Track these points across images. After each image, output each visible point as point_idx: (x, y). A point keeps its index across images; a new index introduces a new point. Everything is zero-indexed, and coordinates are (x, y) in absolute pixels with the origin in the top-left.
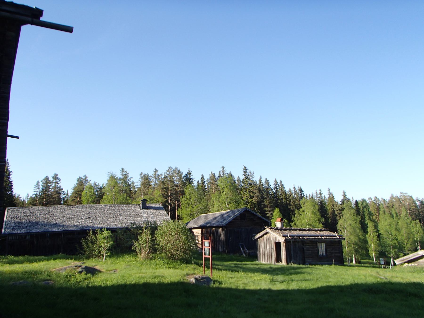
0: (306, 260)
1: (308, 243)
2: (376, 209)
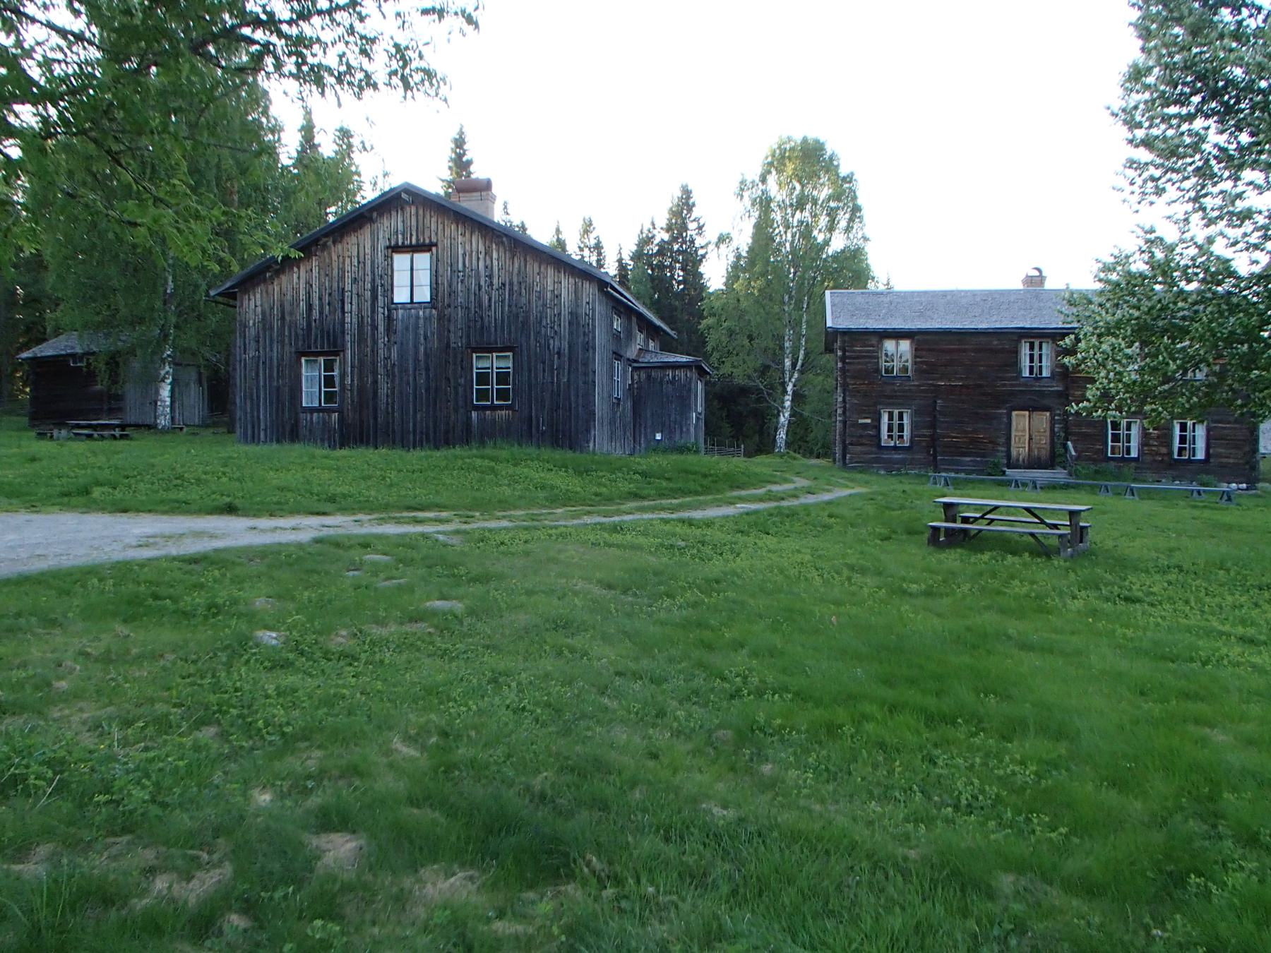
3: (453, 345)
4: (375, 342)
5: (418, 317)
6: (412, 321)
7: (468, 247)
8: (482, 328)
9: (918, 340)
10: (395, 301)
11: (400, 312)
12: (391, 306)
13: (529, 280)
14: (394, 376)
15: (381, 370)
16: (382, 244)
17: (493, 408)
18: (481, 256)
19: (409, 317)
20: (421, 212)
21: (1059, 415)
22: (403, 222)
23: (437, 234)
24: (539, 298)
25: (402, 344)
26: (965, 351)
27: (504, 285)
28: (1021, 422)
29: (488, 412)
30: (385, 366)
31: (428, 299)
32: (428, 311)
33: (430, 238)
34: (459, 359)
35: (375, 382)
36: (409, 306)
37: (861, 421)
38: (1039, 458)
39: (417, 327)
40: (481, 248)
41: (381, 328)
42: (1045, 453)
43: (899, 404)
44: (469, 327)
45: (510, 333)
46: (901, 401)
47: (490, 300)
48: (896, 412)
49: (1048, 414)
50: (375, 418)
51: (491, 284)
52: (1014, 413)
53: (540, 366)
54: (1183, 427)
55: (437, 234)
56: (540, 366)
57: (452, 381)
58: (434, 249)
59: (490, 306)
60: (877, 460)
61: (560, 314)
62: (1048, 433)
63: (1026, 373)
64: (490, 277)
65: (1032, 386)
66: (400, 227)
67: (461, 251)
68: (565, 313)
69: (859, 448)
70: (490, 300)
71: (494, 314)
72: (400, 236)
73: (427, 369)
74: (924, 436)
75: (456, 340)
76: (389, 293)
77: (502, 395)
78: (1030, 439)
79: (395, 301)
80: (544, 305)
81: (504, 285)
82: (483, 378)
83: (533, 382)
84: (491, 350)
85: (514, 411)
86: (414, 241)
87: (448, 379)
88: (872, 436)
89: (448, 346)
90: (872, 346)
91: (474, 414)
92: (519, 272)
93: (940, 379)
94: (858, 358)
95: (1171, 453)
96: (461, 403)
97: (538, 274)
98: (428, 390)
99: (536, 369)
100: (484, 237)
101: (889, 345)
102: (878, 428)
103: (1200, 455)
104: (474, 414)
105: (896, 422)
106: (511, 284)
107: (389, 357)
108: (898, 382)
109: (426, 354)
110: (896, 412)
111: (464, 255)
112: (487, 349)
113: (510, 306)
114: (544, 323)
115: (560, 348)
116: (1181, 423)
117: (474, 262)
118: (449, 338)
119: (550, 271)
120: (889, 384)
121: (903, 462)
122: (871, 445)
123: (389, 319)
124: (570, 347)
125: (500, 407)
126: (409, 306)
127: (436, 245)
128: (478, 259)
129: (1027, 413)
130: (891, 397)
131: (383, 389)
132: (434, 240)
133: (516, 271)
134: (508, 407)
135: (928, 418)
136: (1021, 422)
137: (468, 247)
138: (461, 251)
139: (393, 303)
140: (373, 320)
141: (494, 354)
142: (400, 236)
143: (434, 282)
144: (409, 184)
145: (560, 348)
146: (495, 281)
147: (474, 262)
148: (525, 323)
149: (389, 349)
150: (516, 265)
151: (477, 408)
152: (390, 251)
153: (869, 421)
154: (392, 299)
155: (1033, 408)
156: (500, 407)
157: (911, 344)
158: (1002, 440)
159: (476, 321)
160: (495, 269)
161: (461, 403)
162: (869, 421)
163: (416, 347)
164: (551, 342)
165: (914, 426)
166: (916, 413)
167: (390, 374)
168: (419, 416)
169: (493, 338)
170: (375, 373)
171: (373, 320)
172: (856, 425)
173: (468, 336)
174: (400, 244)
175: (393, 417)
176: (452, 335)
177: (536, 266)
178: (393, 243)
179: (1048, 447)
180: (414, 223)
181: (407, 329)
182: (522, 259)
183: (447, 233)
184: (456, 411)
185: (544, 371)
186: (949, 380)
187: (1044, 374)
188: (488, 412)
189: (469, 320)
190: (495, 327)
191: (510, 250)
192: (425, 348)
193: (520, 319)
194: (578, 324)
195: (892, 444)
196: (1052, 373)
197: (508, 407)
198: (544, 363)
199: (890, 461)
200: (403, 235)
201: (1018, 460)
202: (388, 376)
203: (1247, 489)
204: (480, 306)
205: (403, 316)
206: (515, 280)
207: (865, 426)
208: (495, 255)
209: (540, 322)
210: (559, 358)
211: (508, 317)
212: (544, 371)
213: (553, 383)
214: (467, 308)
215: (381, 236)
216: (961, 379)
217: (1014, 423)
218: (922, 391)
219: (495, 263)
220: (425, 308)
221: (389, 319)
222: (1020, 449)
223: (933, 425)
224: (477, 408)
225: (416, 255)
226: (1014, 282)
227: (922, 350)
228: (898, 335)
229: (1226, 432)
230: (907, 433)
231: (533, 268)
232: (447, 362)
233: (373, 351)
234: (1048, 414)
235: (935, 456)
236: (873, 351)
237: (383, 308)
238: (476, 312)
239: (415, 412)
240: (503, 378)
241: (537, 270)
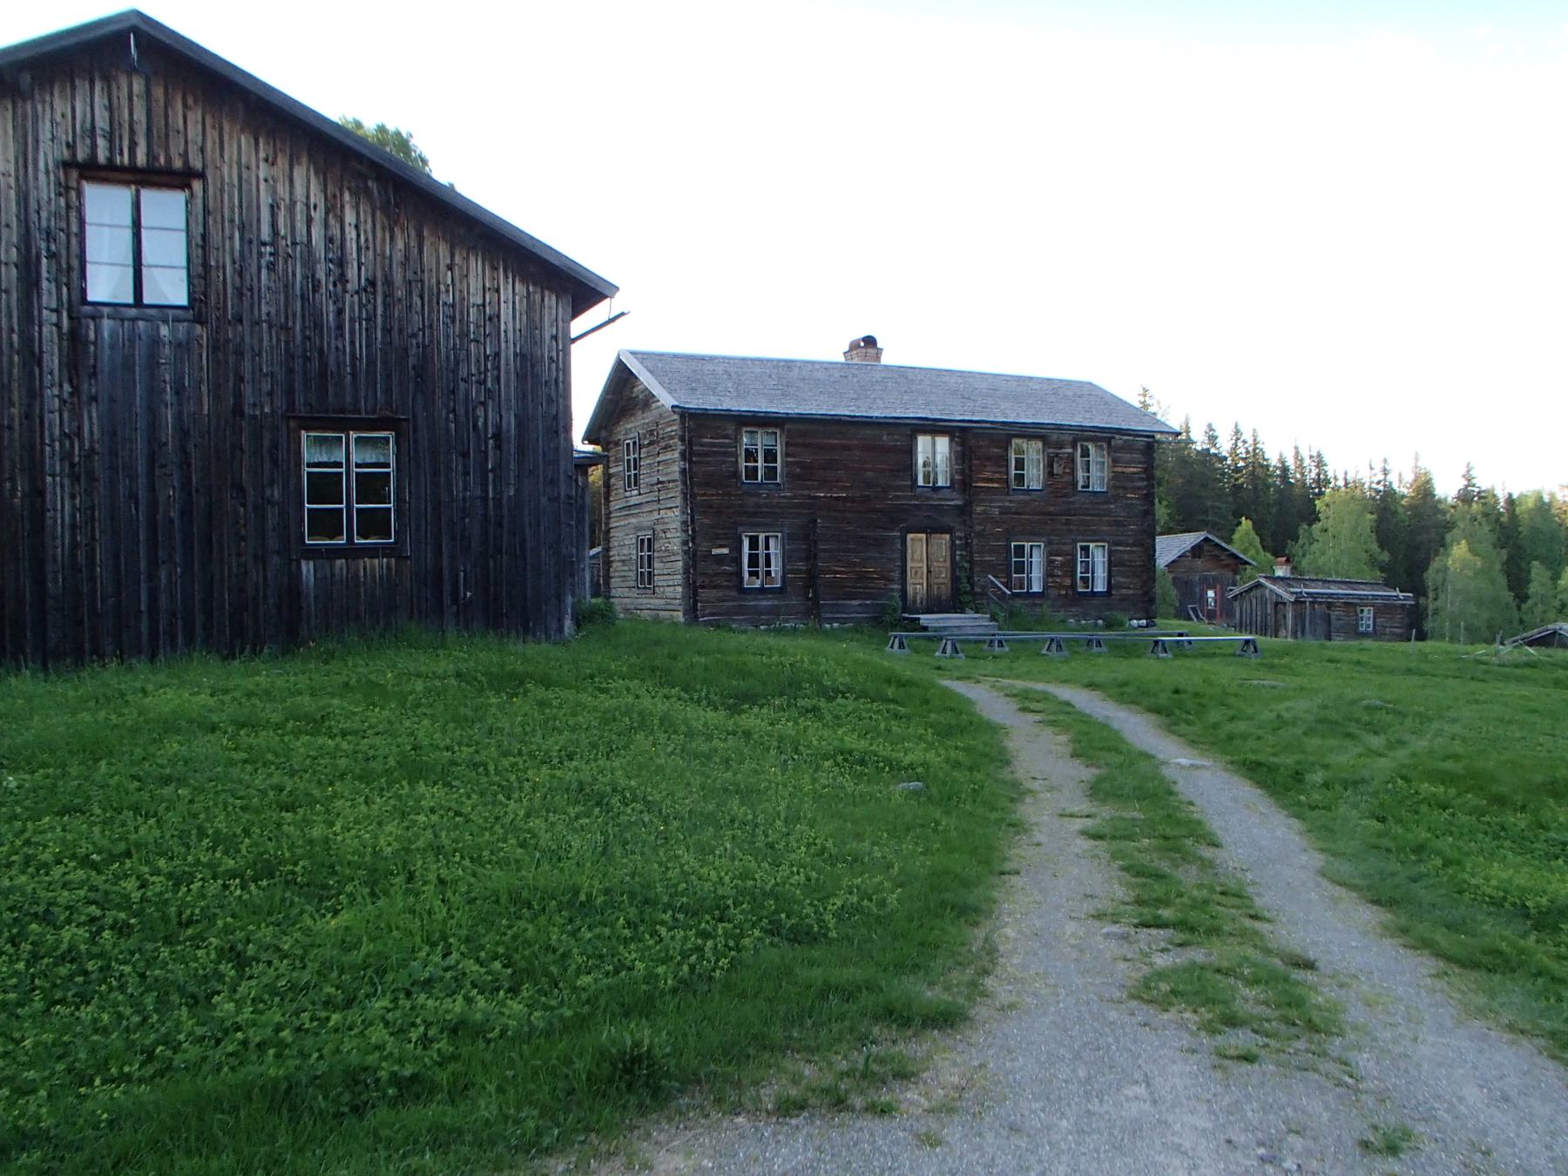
3: (248, 410)
4: (34, 394)
5: (156, 341)
6: (140, 351)
7: (282, 190)
8: (323, 374)
9: (789, 430)
10: (90, 298)
11: (107, 324)
12: (78, 306)
13: (430, 279)
14: (92, 478)
15: (53, 463)
16: (49, 154)
17: (351, 552)
18: (318, 216)
19: (133, 337)
20: (158, 92)
21: (960, 539)
22: (110, 108)
23: (202, 150)
24: (453, 320)
25: (112, 400)
26: (847, 448)
27: (372, 283)
28: (917, 544)
29: (340, 563)
30: (67, 456)
31: (183, 300)
32: (182, 328)
33: (185, 155)
34: (266, 443)
35: (38, 492)
36: (133, 312)
37: (715, 551)
38: (939, 598)
39: (153, 363)
40: (316, 197)
41: (52, 360)
42: (946, 591)
43: (766, 525)
44: (291, 371)
45: (388, 391)
46: (768, 520)
47: (340, 312)
48: (762, 536)
49: (948, 536)
50: (39, 580)
51: (342, 279)
52: (910, 536)
53: (456, 462)
54: (754, 543)
55: (202, 150)
56: (456, 462)
57: (251, 491)
58: (197, 185)
59: (340, 327)
60: (741, 610)
61: (497, 355)
62: (948, 564)
63: (921, 482)
64: (341, 263)
65: (928, 499)
66: (102, 122)
67: (265, 200)
68: (508, 352)
69: (714, 593)
70: (340, 312)
71: (355, 342)
72: (101, 143)
73: (185, 464)
74: (800, 571)
75: (259, 400)
76: (75, 275)
77: (373, 523)
78: (929, 572)
79: (90, 298)
80: (464, 335)
81: (372, 283)
82: (326, 486)
83: (444, 498)
84: (345, 425)
85: (400, 558)
86: (141, 159)
87: (240, 490)
88: (730, 574)
89: (238, 410)
90: (726, 437)
91: (307, 568)
92: (407, 258)
93: (819, 489)
94: (707, 454)
95: (1073, 586)
96: (272, 542)
97: (450, 268)
98: (186, 512)
99: (449, 469)
100: (323, 173)
101: (923, 442)
102: (738, 561)
103: (1100, 587)
104: (307, 568)
105: (761, 551)
106: (388, 282)
107: (79, 434)
108: (764, 493)
109: (183, 433)
110: (762, 536)
111: (274, 208)
112: (335, 421)
113: (387, 331)
114: (463, 372)
115: (499, 427)
116: (750, 537)
117: (301, 226)
118: (238, 395)
119: (476, 266)
120: (752, 495)
121: (774, 612)
122: (728, 587)
123: (75, 340)
124: (519, 424)
125: (372, 552)
126: (133, 312)
127: (202, 176)
128: (309, 221)
129: (924, 536)
130: (755, 514)
131: (61, 504)
132: (197, 164)
133: (398, 256)
134: (387, 551)
135: (804, 547)
136: (917, 544)
137: (282, 190)
138: (265, 200)
139: (84, 301)
140: (27, 339)
141: (353, 435)
142: (101, 143)
143: (198, 261)
144: (138, 14)
145: (499, 427)
146: (352, 273)
147: (301, 226)
148: (422, 370)
149: (76, 415)
150: (400, 245)
151: (313, 553)
152: (74, 174)
153: (725, 551)
154: (84, 292)
155: (931, 530)
156: (372, 552)
157: (951, 441)
158: (896, 575)
159: (307, 359)
160: (352, 247)
161: (272, 542)
162: (725, 551)
163: (152, 411)
164: (480, 412)
165: (787, 558)
166: (789, 538)
167: (79, 474)
168: (163, 574)
169: (348, 399)
170: (35, 470)
171: (27, 339)
172: (708, 556)
173: (290, 392)
174: (102, 156)
175: (92, 578)
176: (247, 390)
177: (443, 250)
178: (81, 155)
179: (948, 581)
180: (140, 115)
181: (128, 366)
182: (413, 233)
183: (230, 151)
184: (261, 559)
185: (466, 473)
186: (831, 490)
187: (940, 483)
188: (340, 563)
189: (290, 356)
190: (354, 375)
191: (385, 209)
192: (179, 417)
193: (412, 361)
194: (536, 377)
195: (758, 584)
196: (952, 481)
197: (387, 551)
198: (466, 455)
199: (759, 611)
200: (111, 141)
201: (915, 601)
202: (75, 478)
203: (1147, 626)
204: (318, 325)
205: (113, 334)
206: (398, 277)
207: (720, 559)
208: (350, 217)
209: (455, 371)
210: (498, 447)
211: (385, 353)
212: (466, 473)
213: (485, 499)
214: (285, 328)
215: (45, 135)
216: (844, 489)
217: (909, 551)
218: (800, 506)
219: (351, 234)
220: (177, 320)
221: (75, 340)
222: (917, 586)
223: (811, 557)
224: (313, 553)
225: (148, 195)
226: (831, 349)
227: (797, 445)
228: (933, 427)
229: (1126, 557)
230: (776, 568)
231: (437, 253)
232: (237, 447)
233: (27, 416)
234: (948, 536)
235: (816, 599)
236: (729, 446)
237: (57, 311)
238: (306, 338)
239: (154, 564)
240: (371, 486)
241: (445, 259)
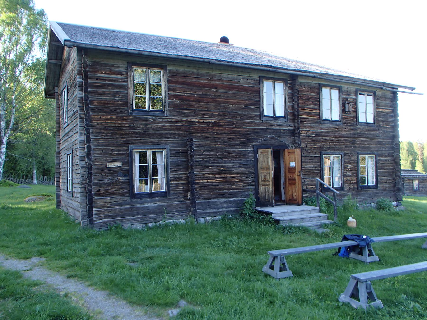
0: (405, 193)
1: (406, 180)
2: (418, 149)
37: (110, 165)
43: (153, 143)
48: (149, 153)
52: (260, 151)
65: (271, 125)
69: (108, 199)
88: (123, 183)
105: (149, 164)
110: (149, 153)
120: (140, 120)
122: (121, 194)
153: (119, 164)
162: (119, 164)
165: (170, 169)
166: (173, 153)
172: (103, 170)
199: (147, 212)
207: (114, 172)
216: (212, 116)
227: (176, 83)
235: (193, 203)
236: (121, 80)
